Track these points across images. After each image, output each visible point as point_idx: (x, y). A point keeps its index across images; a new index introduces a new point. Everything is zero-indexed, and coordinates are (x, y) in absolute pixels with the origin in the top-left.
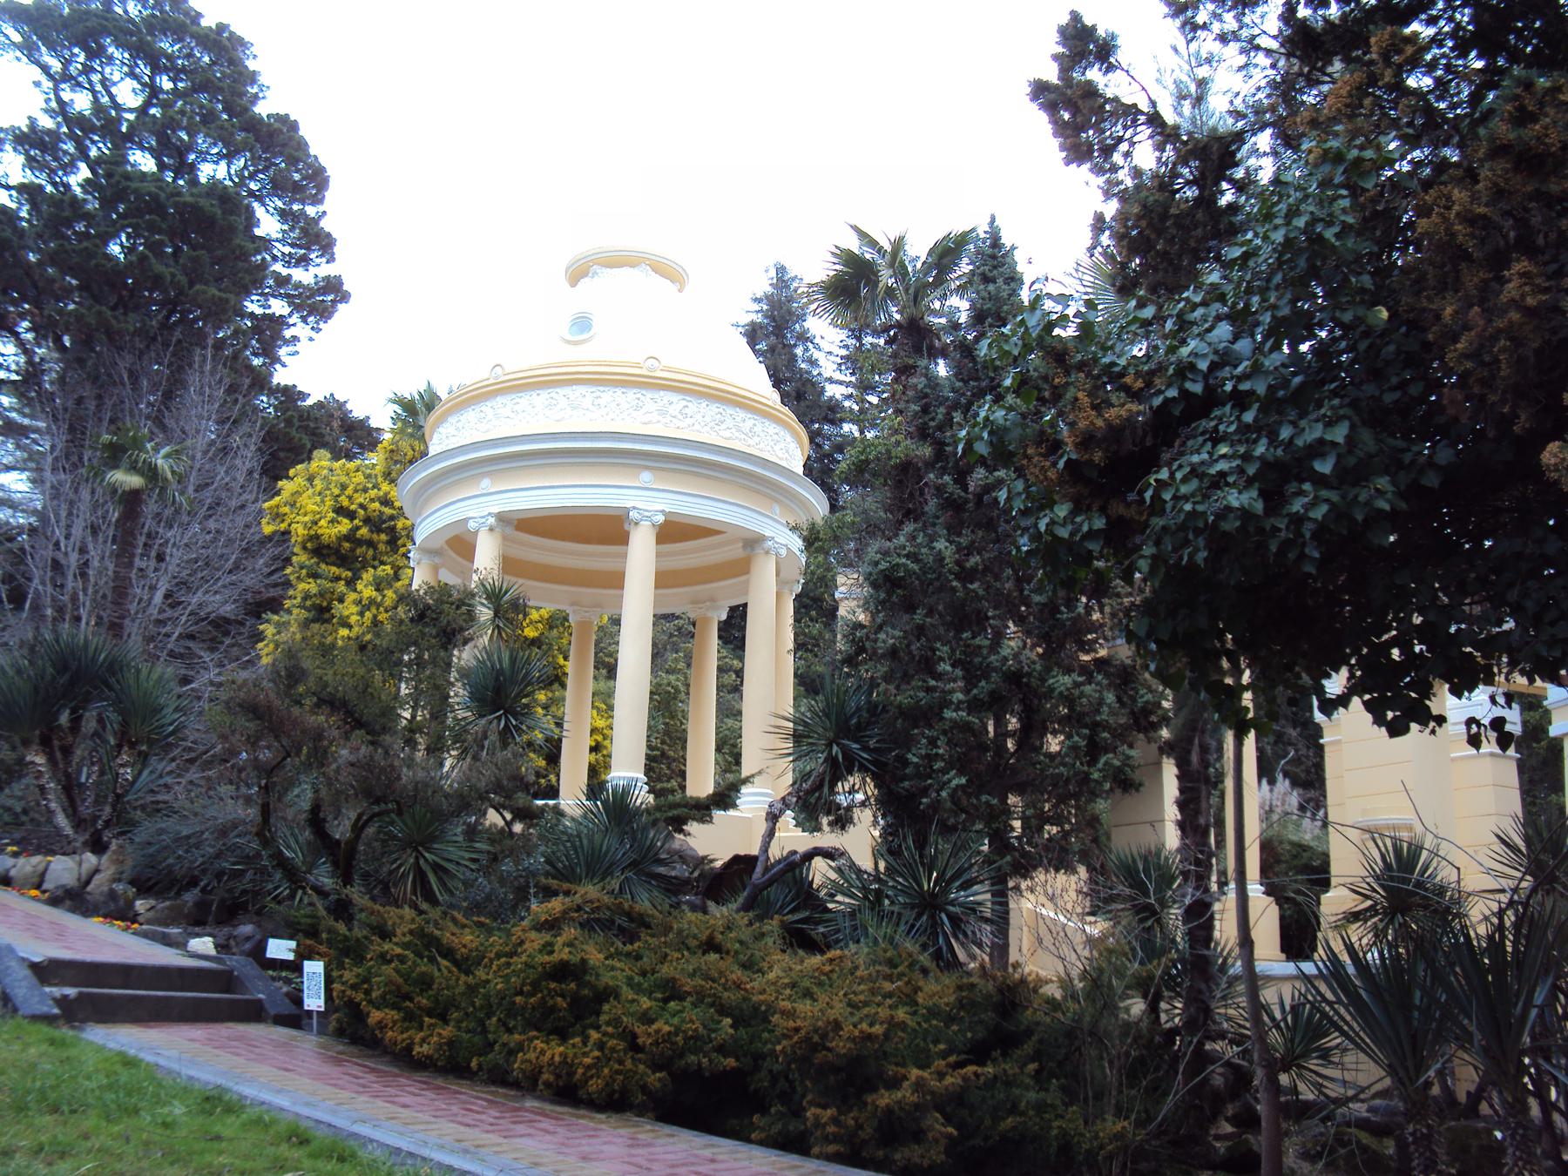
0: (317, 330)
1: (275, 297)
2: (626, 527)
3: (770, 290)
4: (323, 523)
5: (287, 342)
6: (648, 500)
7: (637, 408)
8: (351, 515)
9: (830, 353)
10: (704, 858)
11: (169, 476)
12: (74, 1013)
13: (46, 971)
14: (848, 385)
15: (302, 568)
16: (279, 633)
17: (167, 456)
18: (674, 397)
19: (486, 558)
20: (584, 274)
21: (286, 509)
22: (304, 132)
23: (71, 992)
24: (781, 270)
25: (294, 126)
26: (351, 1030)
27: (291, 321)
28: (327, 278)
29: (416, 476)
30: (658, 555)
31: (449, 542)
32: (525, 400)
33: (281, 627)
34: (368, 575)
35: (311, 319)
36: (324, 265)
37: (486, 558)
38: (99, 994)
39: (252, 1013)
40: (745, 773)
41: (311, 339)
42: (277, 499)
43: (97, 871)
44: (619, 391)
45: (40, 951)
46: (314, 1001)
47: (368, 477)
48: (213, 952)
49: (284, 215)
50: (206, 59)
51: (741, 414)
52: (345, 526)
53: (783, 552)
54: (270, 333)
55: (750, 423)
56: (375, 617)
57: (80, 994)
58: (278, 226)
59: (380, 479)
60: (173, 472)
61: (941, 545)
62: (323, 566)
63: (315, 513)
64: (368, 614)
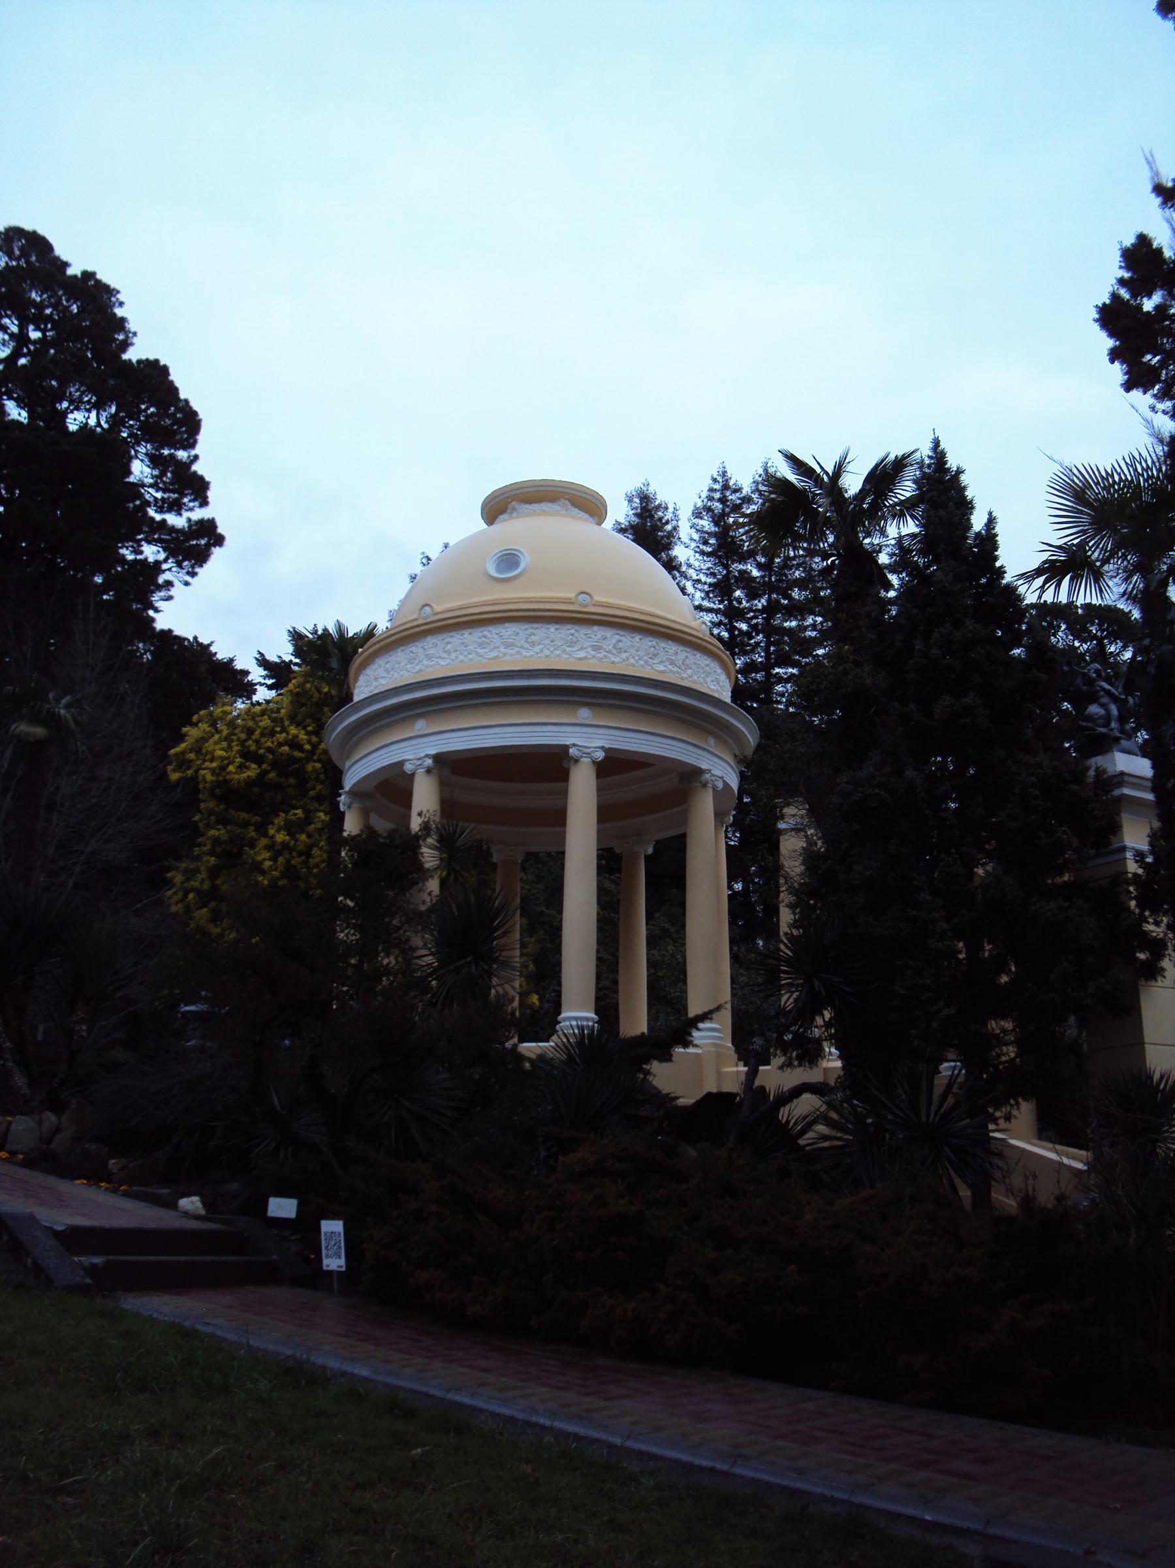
0: (193, 574)
1: (149, 542)
2: (565, 765)
3: (635, 520)
4: (231, 768)
5: (159, 588)
6: (587, 737)
7: (571, 644)
8: (259, 760)
9: (699, 581)
10: (667, 1095)
11: (72, 725)
12: (108, 1282)
13: (75, 1239)
14: (717, 611)
15: (210, 814)
16: (187, 880)
17: (66, 707)
18: (608, 633)
19: (425, 799)
20: (503, 511)
21: (192, 756)
22: (174, 376)
23: (97, 1260)
24: (645, 498)
25: (165, 370)
26: (382, 1291)
27: (165, 566)
28: (201, 522)
29: (341, 723)
30: (599, 789)
31: (377, 787)
32: (455, 639)
33: (190, 874)
34: (280, 820)
35: (186, 563)
36: (197, 510)
37: (425, 799)
38: (131, 1263)
39: (268, 1275)
40: (693, 1010)
41: (187, 584)
42: (183, 745)
43: (58, 1130)
44: (552, 628)
45: (63, 1220)
46: (334, 1262)
47: (274, 720)
48: (203, 1212)
49: (155, 460)
50: (74, 308)
51: (672, 647)
52: (253, 771)
53: (720, 785)
54: (146, 580)
55: (682, 656)
56: (288, 861)
57: (108, 1261)
58: (147, 470)
59: (286, 723)
60: (76, 722)
61: (910, 773)
62: (233, 812)
63: (222, 758)
64: (281, 859)
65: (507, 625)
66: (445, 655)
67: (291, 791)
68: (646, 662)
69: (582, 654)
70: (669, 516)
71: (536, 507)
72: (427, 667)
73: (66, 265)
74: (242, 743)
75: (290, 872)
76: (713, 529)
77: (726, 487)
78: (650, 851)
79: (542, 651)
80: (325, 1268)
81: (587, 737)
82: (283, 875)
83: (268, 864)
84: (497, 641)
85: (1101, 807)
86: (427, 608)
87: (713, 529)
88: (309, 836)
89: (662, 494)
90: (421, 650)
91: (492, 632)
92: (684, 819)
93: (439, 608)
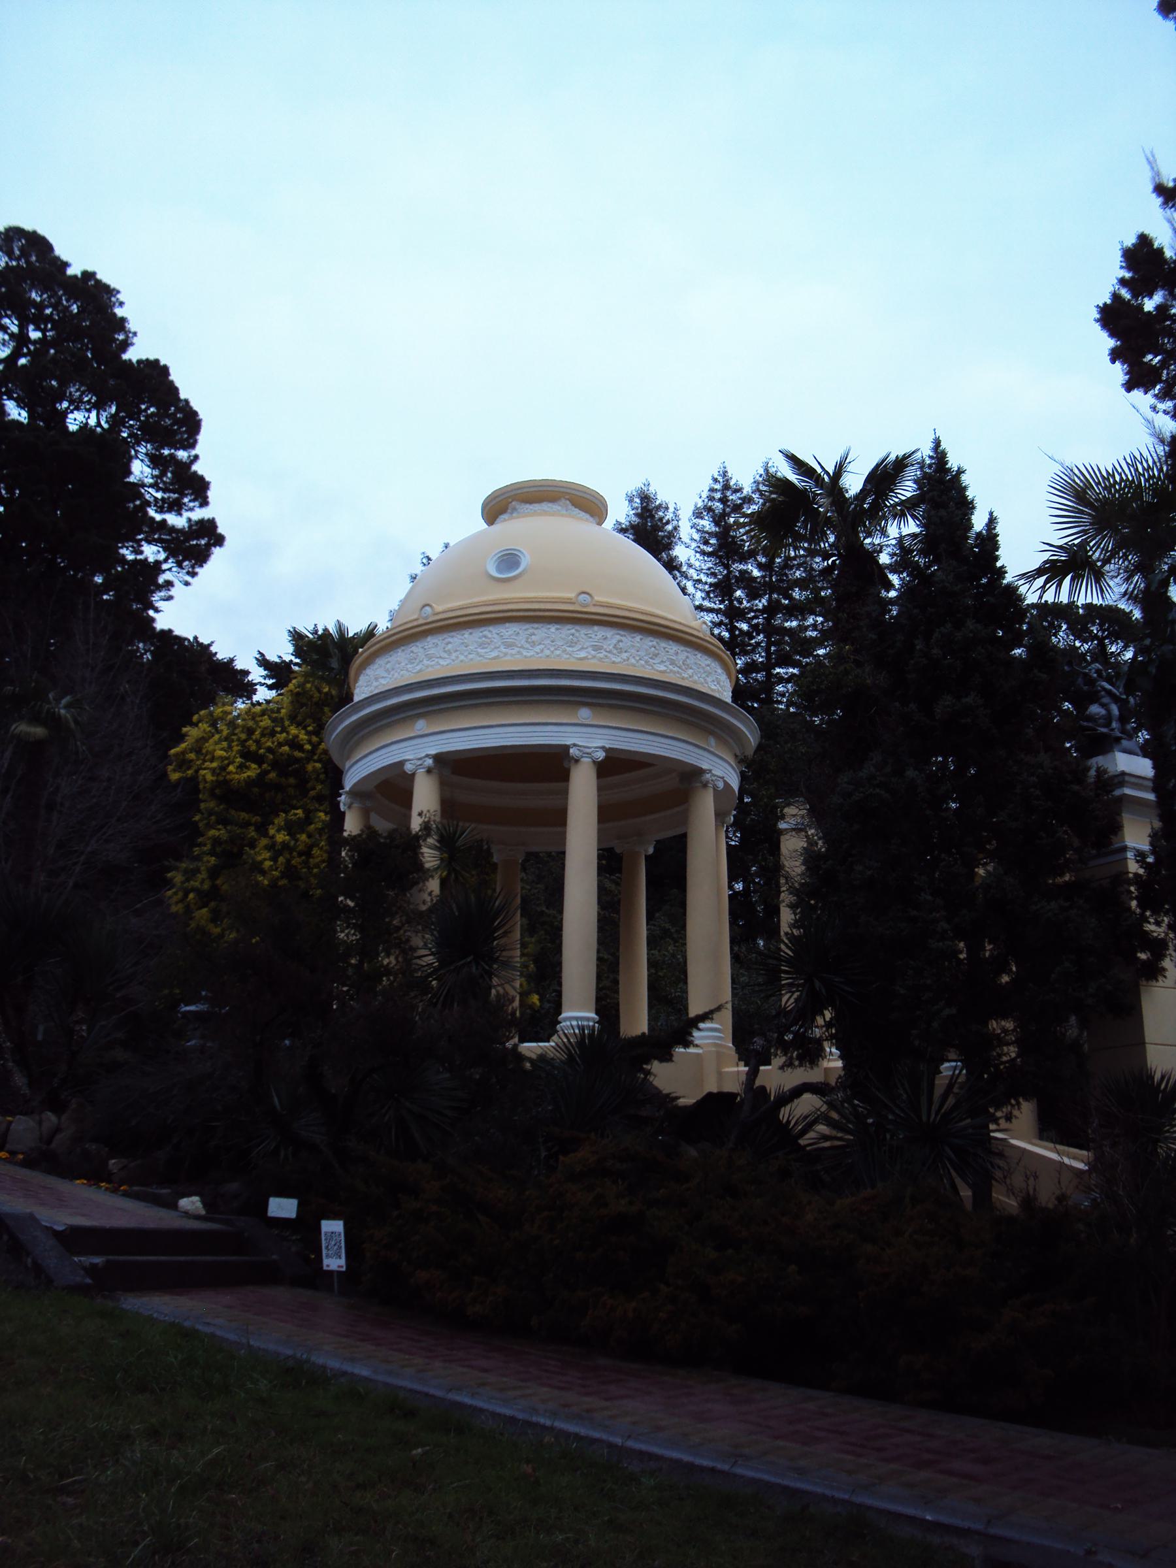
0: (193, 574)
1: (149, 542)
2: (566, 765)
3: (636, 520)
4: (231, 768)
5: (160, 588)
6: (587, 737)
7: (571, 644)
8: (259, 760)
9: (699, 581)
10: (668, 1095)
11: (72, 725)
12: (108, 1282)
13: (75, 1239)
14: (717, 611)
15: (210, 814)
16: (188, 880)
17: (67, 707)
18: (609, 633)
19: (425, 799)
20: (503, 511)
21: (192, 756)
22: (174, 376)
23: (98, 1260)
24: (645, 498)
25: (165, 370)
26: (382, 1291)
27: (165, 566)
28: (201, 522)
29: (342, 723)
30: (600, 789)
31: (378, 787)
32: (456, 639)
33: (190, 874)
34: (280, 820)
35: (186, 563)
36: (198, 510)
37: (425, 799)
38: (131, 1263)
39: (268, 1275)
40: (694, 1010)
41: (187, 584)
42: (183, 745)
43: (58, 1130)
44: (553, 628)
45: (63, 1220)
46: (334, 1262)
47: (274, 720)
48: (203, 1212)
49: (155, 460)
50: (75, 308)
51: (673, 647)
52: (253, 771)
53: (721, 785)
54: (146, 580)
55: (682, 656)
56: (288, 861)
57: (108, 1261)
58: (148, 470)
59: (287, 723)
60: (76, 722)
61: (911, 773)
62: (233, 812)
63: (222, 758)
64: (281, 859)
65: (507, 625)
66: (446, 655)
67: (291, 791)
68: (646, 662)
69: (583, 654)
70: (669, 516)
71: (536, 507)
72: (427, 667)
73: (66, 265)
74: (243, 743)
75: (290, 872)
76: (714, 529)
77: (726, 487)
78: (651, 851)
79: (542, 651)
80: (325, 1268)
81: (587, 737)
82: (284, 875)
83: (268, 864)
84: (497, 641)
85: (1102, 807)
86: (427, 608)
87: (714, 529)
88: (309, 836)
89: (662, 494)
90: (421, 650)
91: (492, 632)
92: (684, 819)
93: (439, 608)
